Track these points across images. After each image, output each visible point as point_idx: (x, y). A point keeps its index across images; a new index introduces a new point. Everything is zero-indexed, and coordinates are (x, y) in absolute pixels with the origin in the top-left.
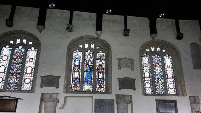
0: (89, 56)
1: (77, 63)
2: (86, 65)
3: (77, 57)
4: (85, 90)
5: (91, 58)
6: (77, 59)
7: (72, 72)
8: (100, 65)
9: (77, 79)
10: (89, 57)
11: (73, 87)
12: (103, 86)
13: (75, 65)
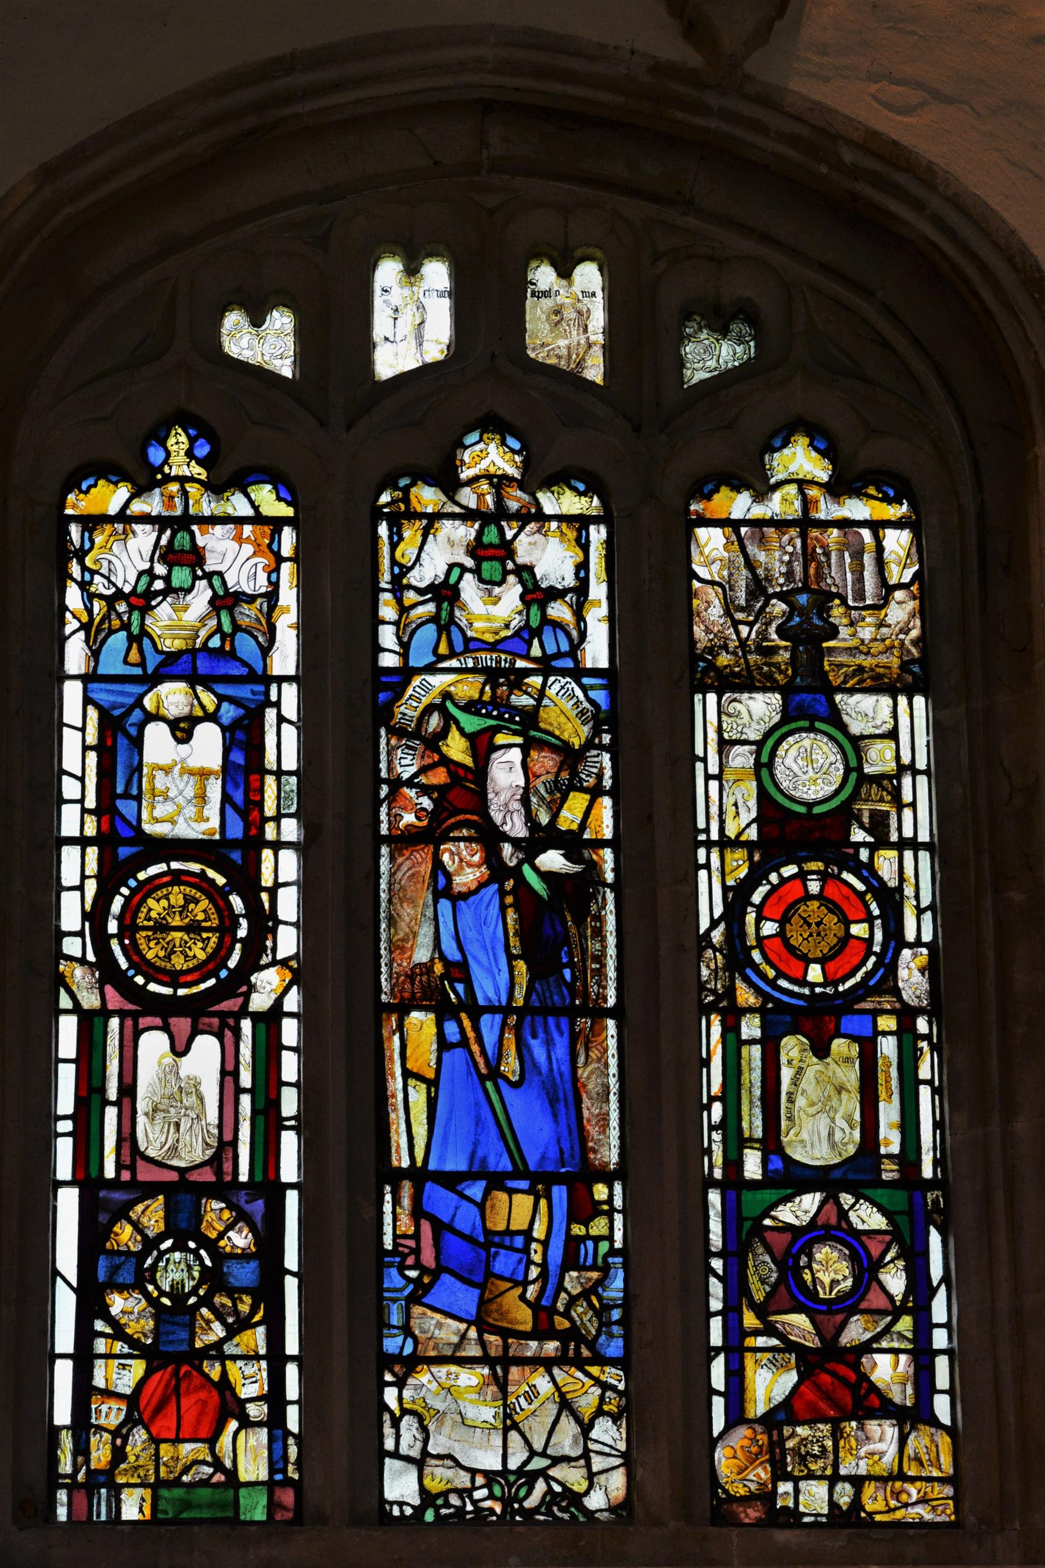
0: (499, 566)
1: (182, 783)
2: (431, 835)
3: (180, 620)
4: (439, 1477)
5: (541, 637)
6: (173, 697)
7: (68, 1028)
8: (788, 832)
9: (215, 1213)
10: (491, 609)
11: (109, 1414)
12: (887, 1370)
13: (124, 848)
